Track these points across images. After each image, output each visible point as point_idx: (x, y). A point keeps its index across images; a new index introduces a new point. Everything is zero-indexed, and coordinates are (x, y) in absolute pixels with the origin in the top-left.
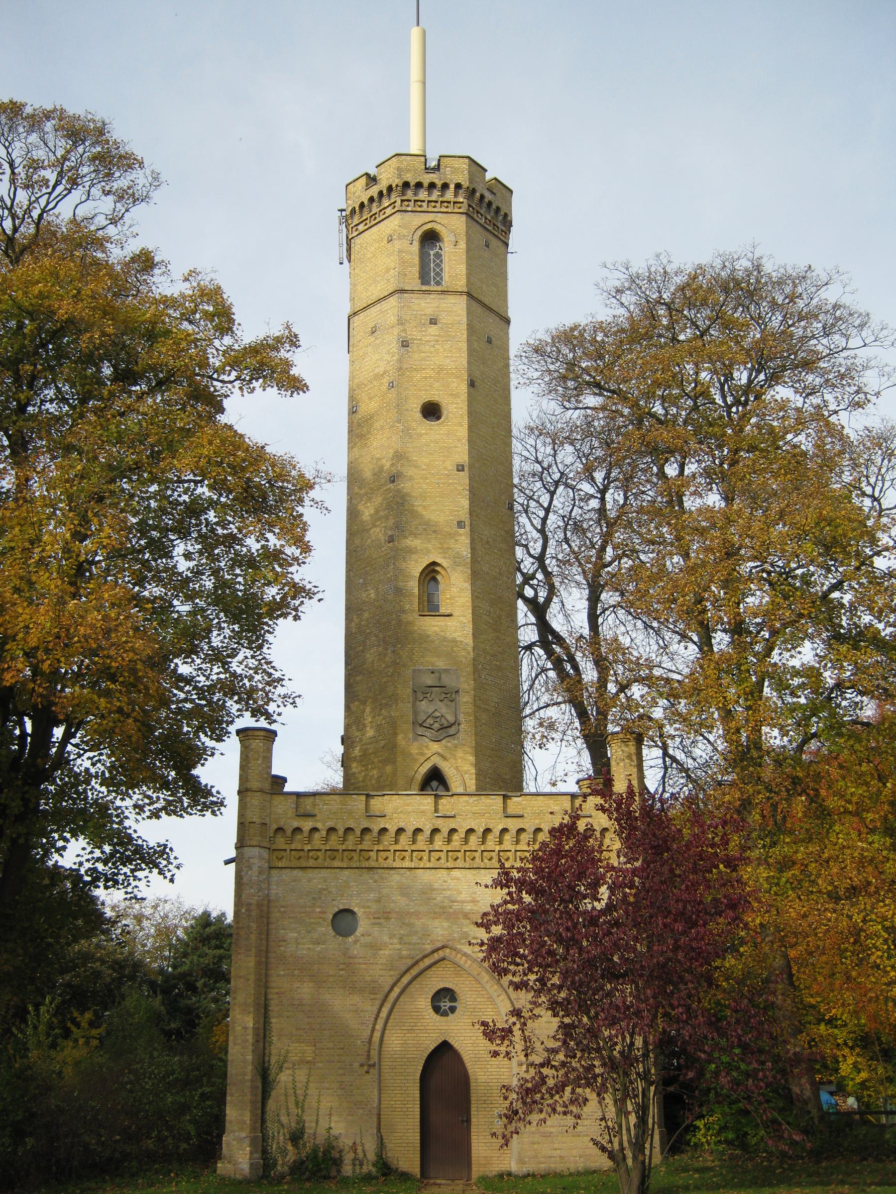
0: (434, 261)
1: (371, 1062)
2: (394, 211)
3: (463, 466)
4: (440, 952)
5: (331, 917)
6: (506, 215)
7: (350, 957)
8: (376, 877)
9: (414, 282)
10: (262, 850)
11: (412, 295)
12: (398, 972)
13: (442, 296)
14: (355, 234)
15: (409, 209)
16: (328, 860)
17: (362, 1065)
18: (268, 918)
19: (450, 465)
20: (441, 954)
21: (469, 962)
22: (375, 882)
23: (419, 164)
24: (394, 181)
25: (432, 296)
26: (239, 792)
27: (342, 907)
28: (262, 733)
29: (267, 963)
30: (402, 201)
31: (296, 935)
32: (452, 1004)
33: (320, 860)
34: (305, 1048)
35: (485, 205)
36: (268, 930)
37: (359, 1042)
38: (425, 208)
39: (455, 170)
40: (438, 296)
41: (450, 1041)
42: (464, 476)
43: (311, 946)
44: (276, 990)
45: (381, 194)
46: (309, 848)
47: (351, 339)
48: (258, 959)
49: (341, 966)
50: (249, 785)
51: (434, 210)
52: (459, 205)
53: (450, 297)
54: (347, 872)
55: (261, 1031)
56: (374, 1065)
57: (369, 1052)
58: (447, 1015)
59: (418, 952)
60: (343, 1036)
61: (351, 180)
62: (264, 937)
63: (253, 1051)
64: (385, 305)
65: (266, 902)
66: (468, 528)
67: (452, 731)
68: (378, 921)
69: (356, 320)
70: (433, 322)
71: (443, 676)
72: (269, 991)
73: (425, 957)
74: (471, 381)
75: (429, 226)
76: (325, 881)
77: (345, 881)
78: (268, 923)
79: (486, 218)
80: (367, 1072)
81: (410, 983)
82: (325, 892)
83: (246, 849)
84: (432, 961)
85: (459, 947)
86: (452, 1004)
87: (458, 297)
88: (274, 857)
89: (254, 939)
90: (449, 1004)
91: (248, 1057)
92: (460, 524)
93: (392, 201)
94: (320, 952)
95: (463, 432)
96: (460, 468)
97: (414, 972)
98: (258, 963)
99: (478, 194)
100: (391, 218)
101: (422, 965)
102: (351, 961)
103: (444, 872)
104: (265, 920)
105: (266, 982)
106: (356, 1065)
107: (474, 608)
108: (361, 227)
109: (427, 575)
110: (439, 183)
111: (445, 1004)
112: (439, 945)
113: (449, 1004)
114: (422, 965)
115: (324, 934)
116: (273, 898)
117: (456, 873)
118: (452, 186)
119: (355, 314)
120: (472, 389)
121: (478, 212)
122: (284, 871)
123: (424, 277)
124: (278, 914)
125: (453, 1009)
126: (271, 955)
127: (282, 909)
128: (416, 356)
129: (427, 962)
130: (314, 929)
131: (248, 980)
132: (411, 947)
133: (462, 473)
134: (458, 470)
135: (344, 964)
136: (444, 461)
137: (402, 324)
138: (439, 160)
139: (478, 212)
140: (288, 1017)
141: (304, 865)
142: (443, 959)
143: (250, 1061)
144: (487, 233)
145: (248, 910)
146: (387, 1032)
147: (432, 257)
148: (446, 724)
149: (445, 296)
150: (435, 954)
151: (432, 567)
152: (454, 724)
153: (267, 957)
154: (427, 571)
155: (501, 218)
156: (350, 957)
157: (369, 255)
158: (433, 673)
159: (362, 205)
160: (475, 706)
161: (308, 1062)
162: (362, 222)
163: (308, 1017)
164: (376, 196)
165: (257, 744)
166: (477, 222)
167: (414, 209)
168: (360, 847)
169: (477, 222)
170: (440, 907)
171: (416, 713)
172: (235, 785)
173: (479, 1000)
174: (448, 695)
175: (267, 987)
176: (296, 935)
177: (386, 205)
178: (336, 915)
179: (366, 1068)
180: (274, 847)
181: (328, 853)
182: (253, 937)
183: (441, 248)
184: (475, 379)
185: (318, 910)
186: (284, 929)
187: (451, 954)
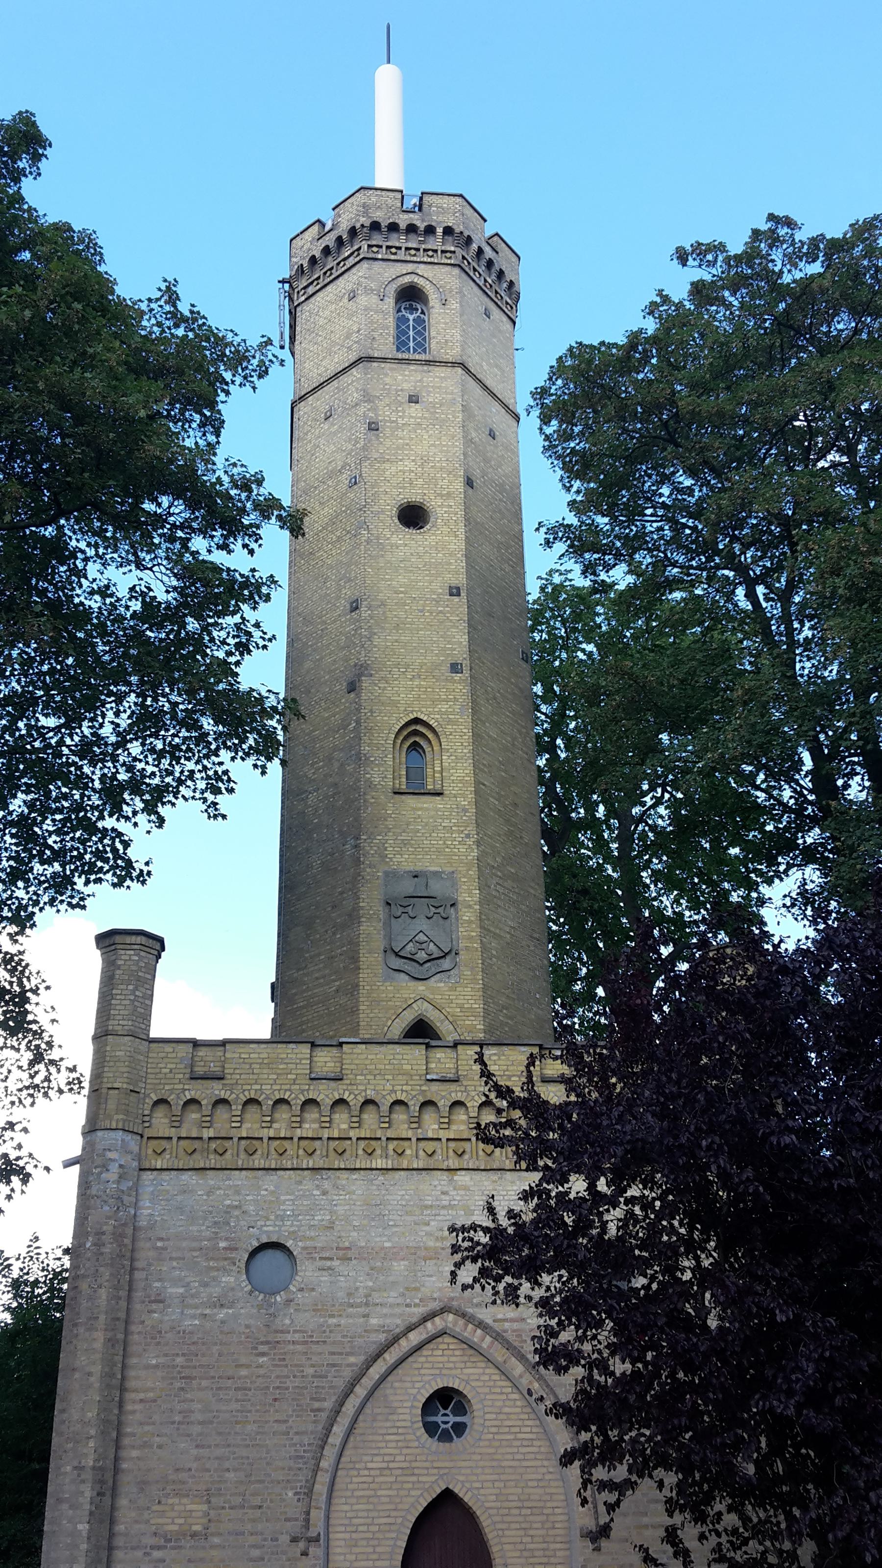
0: (414, 328)
1: (312, 1533)
2: (358, 259)
3: (458, 589)
4: (437, 1320)
5: (246, 1256)
6: (511, 284)
7: (277, 1332)
8: (326, 1185)
9: (386, 346)
10: (128, 1137)
11: (383, 365)
12: (362, 1358)
13: (425, 368)
14: (303, 298)
15: (380, 256)
16: (243, 1155)
17: (294, 1540)
18: (132, 1260)
19: (439, 587)
20: (438, 1323)
21: (488, 1339)
22: (324, 1193)
23: (393, 201)
24: (358, 221)
25: (412, 367)
26: (96, 1038)
27: (265, 1240)
28: (139, 939)
29: (125, 1343)
30: (370, 246)
31: (181, 1290)
32: (458, 1419)
33: (228, 1155)
34: (189, 1507)
35: (483, 262)
36: (131, 1282)
37: (290, 1494)
38: (401, 255)
39: (443, 211)
40: (420, 368)
41: (456, 1491)
42: (460, 604)
43: (207, 1311)
44: (142, 1396)
45: (339, 240)
46: (211, 1135)
47: (296, 433)
48: (110, 1334)
49: (263, 1348)
50: (112, 1025)
51: (415, 259)
52: (448, 255)
53: (437, 369)
54: (274, 1177)
55: (109, 1476)
56: (317, 1539)
57: (308, 1513)
58: (451, 1440)
59: (399, 1321)
60: (261, 1482)
61: (299, 231)
62: (123, 1294)
63: (91, 1513)
64: (345, 379)
65: (129, 1231)
66: (467, 673)
67: (446, 964)
68: (328, 1263)
69: (303, 408)
70: (414, 399)
71: (431, 882)
72: (123, 1454)
73: (410, 1328)
74: (468, 479)
75: (407, 279)
76: (238, 1193)
77: (273, 1192)
78: (132, 1269)
79: (485, 281)
80: (305, 1554)
81: (383, 1378)
82: (236, 1213)
83: (100, 1134)
84: (424, 1336)
85: (470, 1310)
86: (458, 1419)
87: (449, 369)
88: (150, 1151)
89: (104, 1297)
90: (452, 1419)
91: (80, 1527)
92: (455, 668)
93: (356, 247)
94: (223, 1322)
95: (458, 545)
96: (455, 592)
97: (391, 1357)
98: (111, 1342)
99: (475, 246)
100: (354, 270)
101: (405, 1345)
102: (280, 1337)
103: (445, 1176)
104: (127, 1263)
105: (123, 1378)
106: (285, 1539)
107: (478, 783)
108: (311, 290)
109: (406, 738)
110: (422, 226)
111: (446, 1418)
112: (434, 1306)
113: (452, 1419)
114: (405, 1345)
115: (233, 1289)
116: (143, 1223)
117: (462, 1178)
118: (440, 230)
119: (302, 398)
120: (470, 491)
121: (475, 270)
122: (165, 1176)
123: (401, 344)
124: (151, 1254)
125: (460, 1429)
126: (134, 1328)
127: (159, 1244)
128: (388, 443)
129: (415, 1338)
130: (214, 1279)
131: (90, 1374)
132: (385, 1311)
133: (456, 599)
134: (451, 595)
135: (267, 1343)
136: (431, 582)
137: (369, 401)
138: (421, 199)
139: (475, 270)
140: (160, 1447)
141: (202, 1165)
142: (443, 1333)
143: (85, 1534)
144: (487, 300)
145: (98, 1244)
146: (339, 1473)
147: (411, 323)
148: (437, 953)
149: (431, 368)
150: (429, 1324)
151: (413, 727)
152: (450, 951)
153: (127, 1332)
154: (405, 733)
155: (505, 285)
156: (277, 1332)
157: (322, 322)
158: (416, 876)
159: (313, 260)
160: (481, 927)
161: (194, 1535)
162: (312, 283)
163: (197, 1446)
164: (332, 244)
165: (127, 957)
166: (474, 281)
167: (386, 257)
168: (299, 1133)
169: (474, 281)
170: (437, 1239)
171: (389, 937)
172: (88, 1025)
173: (506, 1410)
174: (440, 910)
175: (123, 1389)
176: (181, 1290)
177: (347, 254)
178: (254, 1253)
179: (302, 1545)
180: (148, 1133)
181: (243, 1142)
182: (103, 1293)
183: (423, 313)
184: (474, 478)
185: (222, 1244)
186: (160, 1280)
187: (455, 1323)
